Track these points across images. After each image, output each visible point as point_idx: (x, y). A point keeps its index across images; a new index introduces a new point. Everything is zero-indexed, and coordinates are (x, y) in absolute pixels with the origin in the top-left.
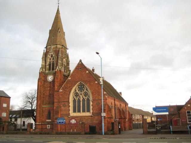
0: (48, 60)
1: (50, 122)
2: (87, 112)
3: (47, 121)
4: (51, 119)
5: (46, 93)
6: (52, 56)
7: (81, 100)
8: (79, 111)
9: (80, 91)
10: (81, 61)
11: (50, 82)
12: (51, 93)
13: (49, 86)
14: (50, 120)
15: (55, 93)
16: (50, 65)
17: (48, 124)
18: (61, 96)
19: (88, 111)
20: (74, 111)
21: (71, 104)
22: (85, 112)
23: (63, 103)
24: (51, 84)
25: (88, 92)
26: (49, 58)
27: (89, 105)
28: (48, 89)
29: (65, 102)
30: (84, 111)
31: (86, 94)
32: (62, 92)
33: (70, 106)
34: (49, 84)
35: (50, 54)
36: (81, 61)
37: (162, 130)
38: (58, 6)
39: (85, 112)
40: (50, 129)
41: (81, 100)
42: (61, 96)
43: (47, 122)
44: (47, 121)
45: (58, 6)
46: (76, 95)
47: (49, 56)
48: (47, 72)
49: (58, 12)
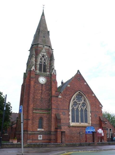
0: (39, 60)
1: (42, 132)
2: (76, 122)
3: (38, 130)
4: (44, 127)
5: (37, 96)
6: (43, 56)
7: (80, 109)
8: (78, 121)
9: (78, 101)
10: (78, 71)
11: (42, 85)
12: (43, 97)
13: (41, 88)
14: (43, 130)
15: (54, 99)
16: (40, 65)
17: (40, 134)
18: (60, 103)
19: (86, 122)
20: (73, 121)
21: (89, 114)
22: (75, 122)
23: (62, 111)
24: (43, 87)
25: (87, 103)
26: (40, 57)
27: (72, 116)
28: (40, 92)
29: (64, 110)
30: (82, 121)
31: (84, 104)
32: (61, 98)
33: (69, 115)
34: (41, 86)
35: (43, 53)
36: (78, 71)
37: (7, 134)
38: (43, 10)
39: (75, 122)
40: (43, 140)
41: (80, 109)
42: (60, 103)
43: (38, 131)
44: (38, 130)
45: (43, 10)
46: (75, 104)
47: (40, 55)
48: (38, 71)
49: (43, 15)
